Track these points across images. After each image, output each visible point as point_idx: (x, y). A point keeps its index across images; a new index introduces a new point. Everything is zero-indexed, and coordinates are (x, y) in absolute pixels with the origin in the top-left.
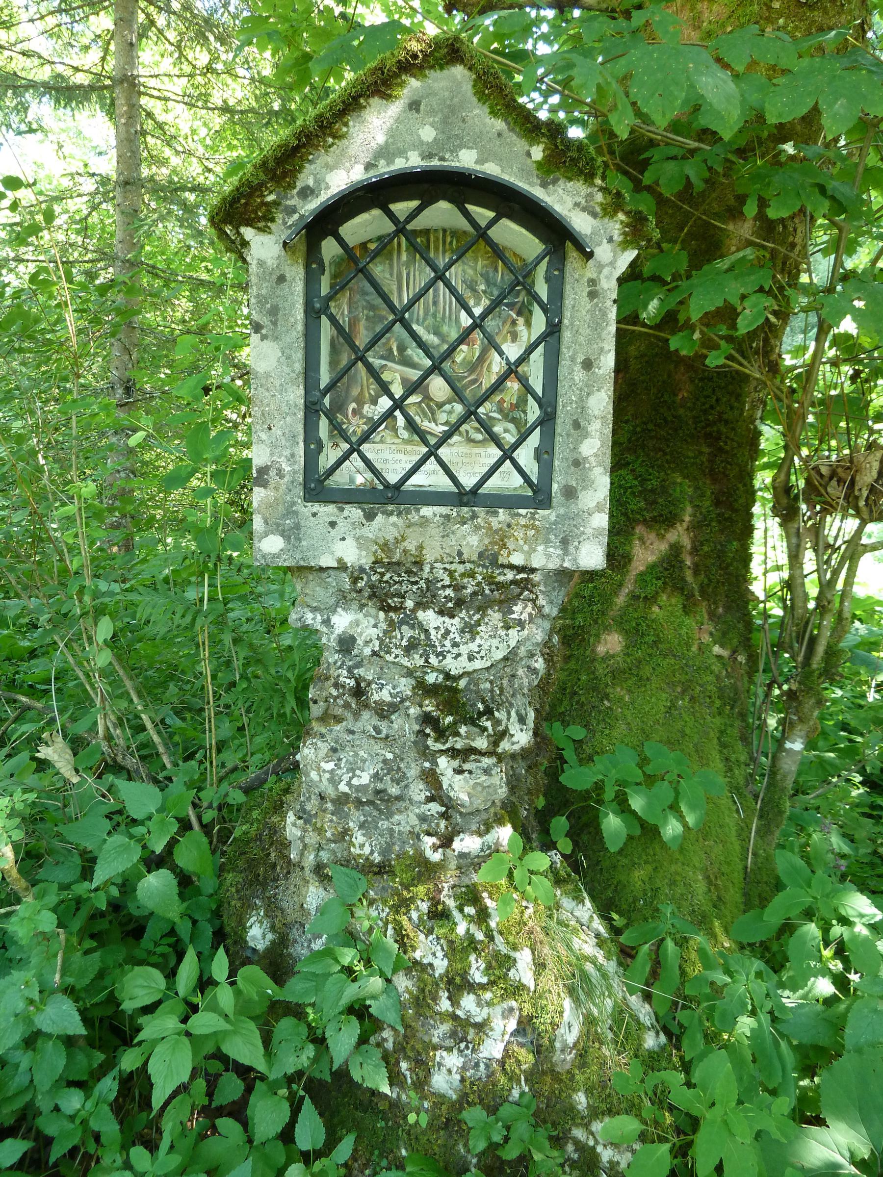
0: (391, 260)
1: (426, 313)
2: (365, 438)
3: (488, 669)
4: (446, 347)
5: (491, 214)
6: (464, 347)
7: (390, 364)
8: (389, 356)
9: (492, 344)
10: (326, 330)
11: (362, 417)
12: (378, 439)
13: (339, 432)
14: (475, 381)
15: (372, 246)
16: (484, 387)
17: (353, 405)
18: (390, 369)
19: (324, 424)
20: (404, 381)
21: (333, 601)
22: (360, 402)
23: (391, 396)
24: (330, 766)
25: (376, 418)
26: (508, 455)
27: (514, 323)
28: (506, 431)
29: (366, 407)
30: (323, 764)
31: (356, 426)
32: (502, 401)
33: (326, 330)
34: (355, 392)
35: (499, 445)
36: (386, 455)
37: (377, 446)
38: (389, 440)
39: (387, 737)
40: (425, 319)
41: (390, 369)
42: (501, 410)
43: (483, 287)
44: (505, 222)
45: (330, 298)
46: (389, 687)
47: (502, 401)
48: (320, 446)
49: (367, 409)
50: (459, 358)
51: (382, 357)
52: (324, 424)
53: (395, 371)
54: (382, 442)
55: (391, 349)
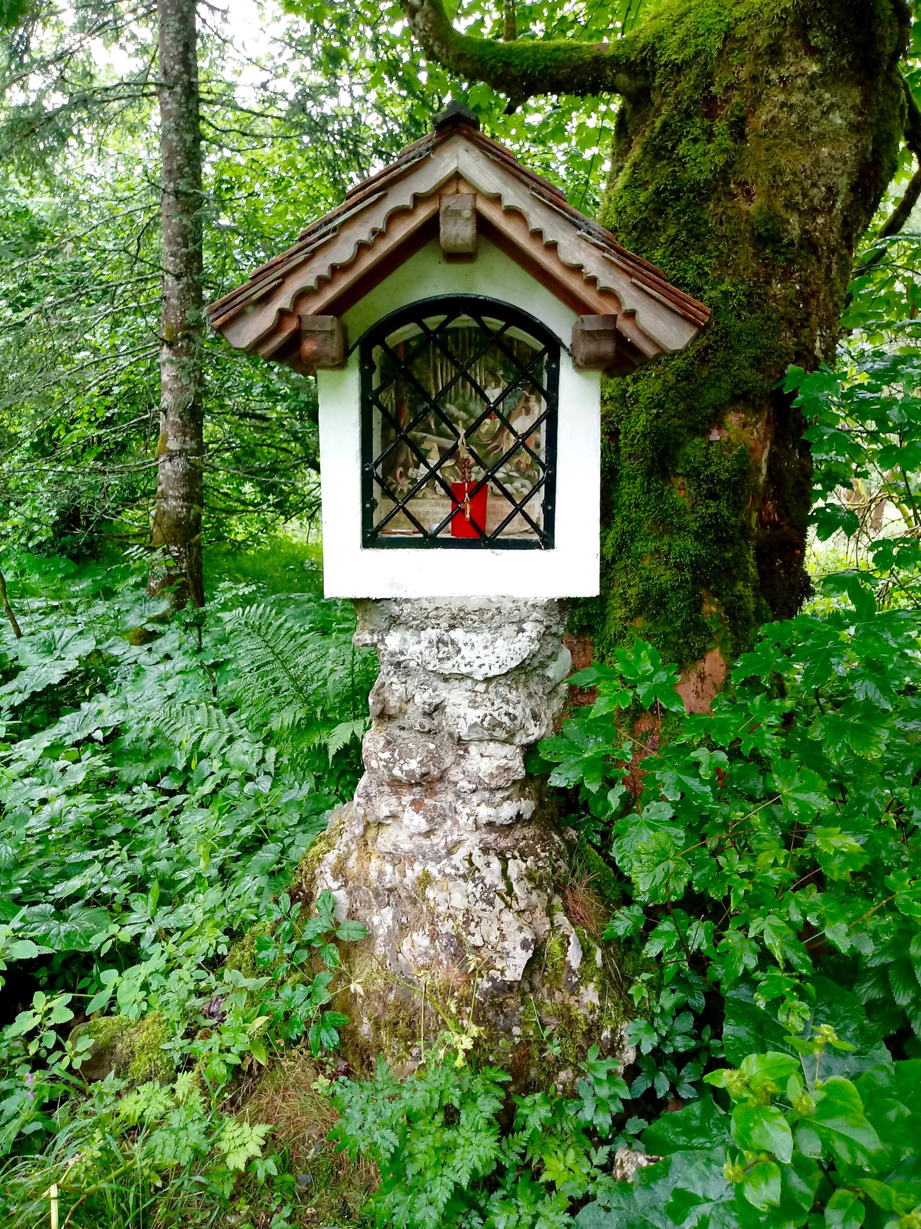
0: (428, 354)
1: (457, 394)
2: (412, 495)
3: (505, 675)
4: (473, 421)
5: (503, 323)
6: (487, 421)
7: (429, 436)
8: (428, 430)
9: (506, 424)
10: (377, 415)
11: (408, 478)
12: (420, 495)
13: (388, 493)
14: (497, 447)
15: (414, 344)
16: (504, 452)
17: (400, 469)
18: (430, 440)
19: (377, 489)
20: (441, 449)
21: (386, 625)
22: (406, 468)
23: (427, 465)
24: (387, 755)
25: (419, 480)
26: (519, 508)
27: (527, 400)
28: (523, 486)
29: (411, 470)
30: (380, 754)
31: (405, 485)
32: (519, 462)
33: (377, 415)
34: (402, 459)
35: (513, 502)
36: (428, 508)
37: (420, 501)
38: (429, 496)
39: (430, 731)
40: (456, 399)
41: (430, 440)
42: (518, 470)
43: (501, 372)
44: (513, 328)
45: (380, 390)
46: (430, 691)
47: (519, 462)
48: (374, 504)
49: (412, 472)
50: (483, 429)
51: (422, 431)
52: (377, 489)
53: (433, 441)
54: (424, 497)
55: (429, 424)
